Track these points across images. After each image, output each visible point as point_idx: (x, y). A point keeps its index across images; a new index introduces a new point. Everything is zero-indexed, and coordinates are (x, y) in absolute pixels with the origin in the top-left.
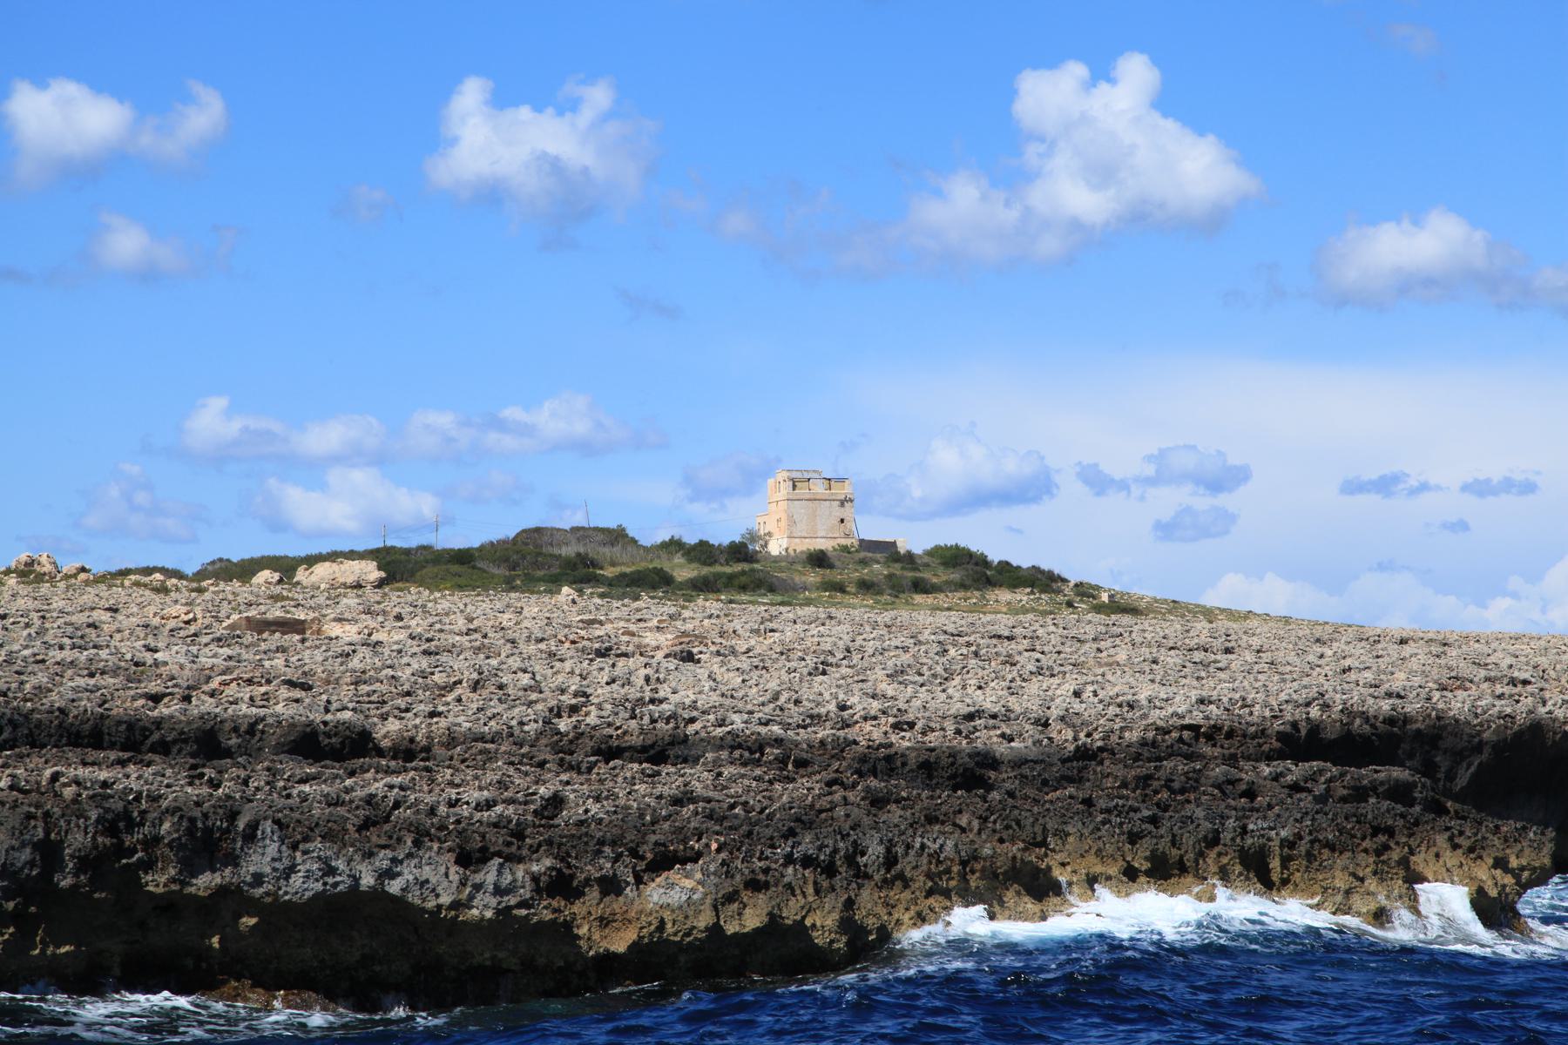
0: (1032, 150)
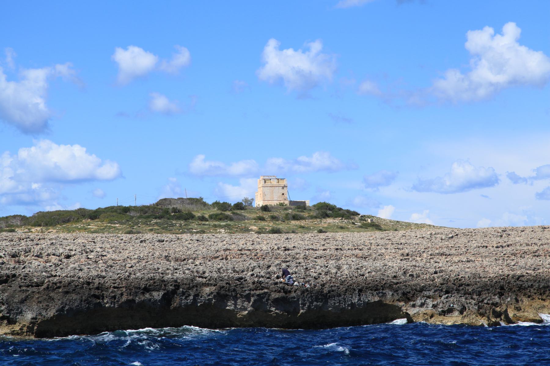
0: (472, 61)
